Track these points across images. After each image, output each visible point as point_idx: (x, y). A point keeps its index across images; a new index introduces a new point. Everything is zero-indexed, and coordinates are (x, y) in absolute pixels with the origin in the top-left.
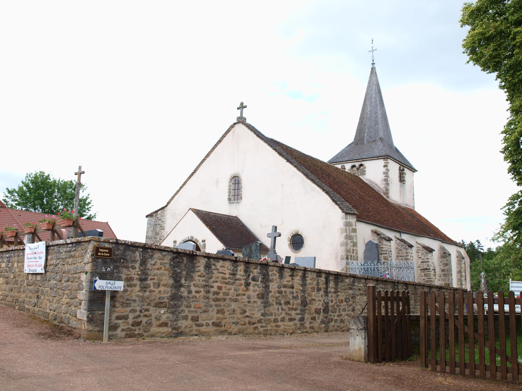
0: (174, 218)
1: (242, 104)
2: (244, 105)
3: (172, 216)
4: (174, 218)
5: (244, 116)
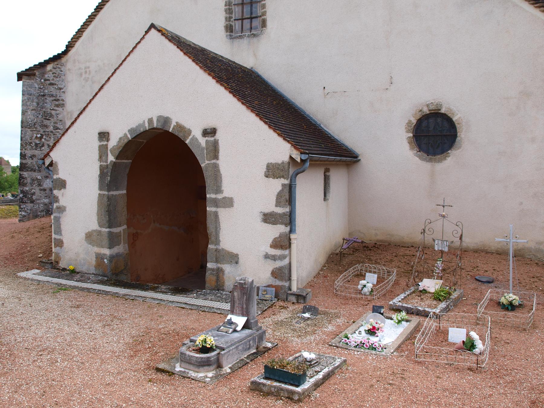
0: (86, 80)
3: (81, 75)
4: (86, 80)
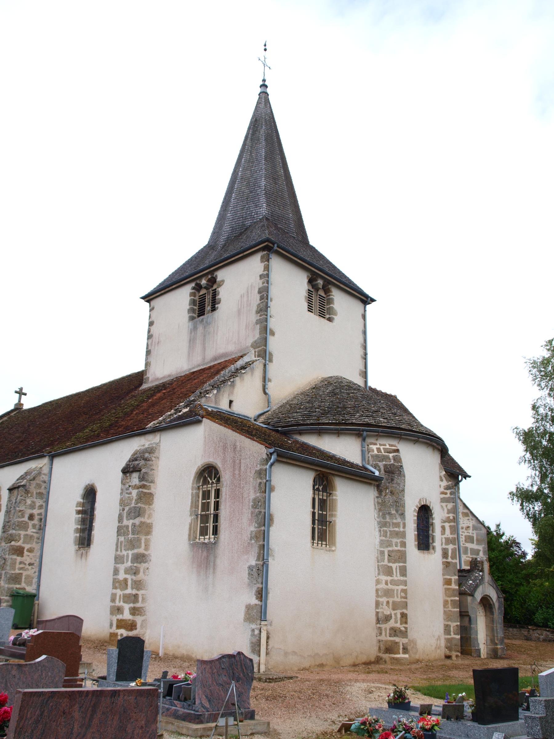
1: (21, 389)
2: (18, 390)
5: (22, 402)
